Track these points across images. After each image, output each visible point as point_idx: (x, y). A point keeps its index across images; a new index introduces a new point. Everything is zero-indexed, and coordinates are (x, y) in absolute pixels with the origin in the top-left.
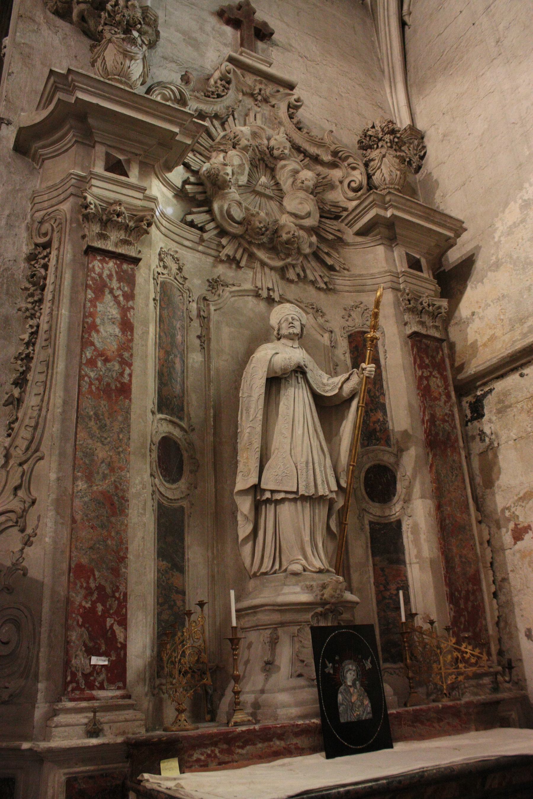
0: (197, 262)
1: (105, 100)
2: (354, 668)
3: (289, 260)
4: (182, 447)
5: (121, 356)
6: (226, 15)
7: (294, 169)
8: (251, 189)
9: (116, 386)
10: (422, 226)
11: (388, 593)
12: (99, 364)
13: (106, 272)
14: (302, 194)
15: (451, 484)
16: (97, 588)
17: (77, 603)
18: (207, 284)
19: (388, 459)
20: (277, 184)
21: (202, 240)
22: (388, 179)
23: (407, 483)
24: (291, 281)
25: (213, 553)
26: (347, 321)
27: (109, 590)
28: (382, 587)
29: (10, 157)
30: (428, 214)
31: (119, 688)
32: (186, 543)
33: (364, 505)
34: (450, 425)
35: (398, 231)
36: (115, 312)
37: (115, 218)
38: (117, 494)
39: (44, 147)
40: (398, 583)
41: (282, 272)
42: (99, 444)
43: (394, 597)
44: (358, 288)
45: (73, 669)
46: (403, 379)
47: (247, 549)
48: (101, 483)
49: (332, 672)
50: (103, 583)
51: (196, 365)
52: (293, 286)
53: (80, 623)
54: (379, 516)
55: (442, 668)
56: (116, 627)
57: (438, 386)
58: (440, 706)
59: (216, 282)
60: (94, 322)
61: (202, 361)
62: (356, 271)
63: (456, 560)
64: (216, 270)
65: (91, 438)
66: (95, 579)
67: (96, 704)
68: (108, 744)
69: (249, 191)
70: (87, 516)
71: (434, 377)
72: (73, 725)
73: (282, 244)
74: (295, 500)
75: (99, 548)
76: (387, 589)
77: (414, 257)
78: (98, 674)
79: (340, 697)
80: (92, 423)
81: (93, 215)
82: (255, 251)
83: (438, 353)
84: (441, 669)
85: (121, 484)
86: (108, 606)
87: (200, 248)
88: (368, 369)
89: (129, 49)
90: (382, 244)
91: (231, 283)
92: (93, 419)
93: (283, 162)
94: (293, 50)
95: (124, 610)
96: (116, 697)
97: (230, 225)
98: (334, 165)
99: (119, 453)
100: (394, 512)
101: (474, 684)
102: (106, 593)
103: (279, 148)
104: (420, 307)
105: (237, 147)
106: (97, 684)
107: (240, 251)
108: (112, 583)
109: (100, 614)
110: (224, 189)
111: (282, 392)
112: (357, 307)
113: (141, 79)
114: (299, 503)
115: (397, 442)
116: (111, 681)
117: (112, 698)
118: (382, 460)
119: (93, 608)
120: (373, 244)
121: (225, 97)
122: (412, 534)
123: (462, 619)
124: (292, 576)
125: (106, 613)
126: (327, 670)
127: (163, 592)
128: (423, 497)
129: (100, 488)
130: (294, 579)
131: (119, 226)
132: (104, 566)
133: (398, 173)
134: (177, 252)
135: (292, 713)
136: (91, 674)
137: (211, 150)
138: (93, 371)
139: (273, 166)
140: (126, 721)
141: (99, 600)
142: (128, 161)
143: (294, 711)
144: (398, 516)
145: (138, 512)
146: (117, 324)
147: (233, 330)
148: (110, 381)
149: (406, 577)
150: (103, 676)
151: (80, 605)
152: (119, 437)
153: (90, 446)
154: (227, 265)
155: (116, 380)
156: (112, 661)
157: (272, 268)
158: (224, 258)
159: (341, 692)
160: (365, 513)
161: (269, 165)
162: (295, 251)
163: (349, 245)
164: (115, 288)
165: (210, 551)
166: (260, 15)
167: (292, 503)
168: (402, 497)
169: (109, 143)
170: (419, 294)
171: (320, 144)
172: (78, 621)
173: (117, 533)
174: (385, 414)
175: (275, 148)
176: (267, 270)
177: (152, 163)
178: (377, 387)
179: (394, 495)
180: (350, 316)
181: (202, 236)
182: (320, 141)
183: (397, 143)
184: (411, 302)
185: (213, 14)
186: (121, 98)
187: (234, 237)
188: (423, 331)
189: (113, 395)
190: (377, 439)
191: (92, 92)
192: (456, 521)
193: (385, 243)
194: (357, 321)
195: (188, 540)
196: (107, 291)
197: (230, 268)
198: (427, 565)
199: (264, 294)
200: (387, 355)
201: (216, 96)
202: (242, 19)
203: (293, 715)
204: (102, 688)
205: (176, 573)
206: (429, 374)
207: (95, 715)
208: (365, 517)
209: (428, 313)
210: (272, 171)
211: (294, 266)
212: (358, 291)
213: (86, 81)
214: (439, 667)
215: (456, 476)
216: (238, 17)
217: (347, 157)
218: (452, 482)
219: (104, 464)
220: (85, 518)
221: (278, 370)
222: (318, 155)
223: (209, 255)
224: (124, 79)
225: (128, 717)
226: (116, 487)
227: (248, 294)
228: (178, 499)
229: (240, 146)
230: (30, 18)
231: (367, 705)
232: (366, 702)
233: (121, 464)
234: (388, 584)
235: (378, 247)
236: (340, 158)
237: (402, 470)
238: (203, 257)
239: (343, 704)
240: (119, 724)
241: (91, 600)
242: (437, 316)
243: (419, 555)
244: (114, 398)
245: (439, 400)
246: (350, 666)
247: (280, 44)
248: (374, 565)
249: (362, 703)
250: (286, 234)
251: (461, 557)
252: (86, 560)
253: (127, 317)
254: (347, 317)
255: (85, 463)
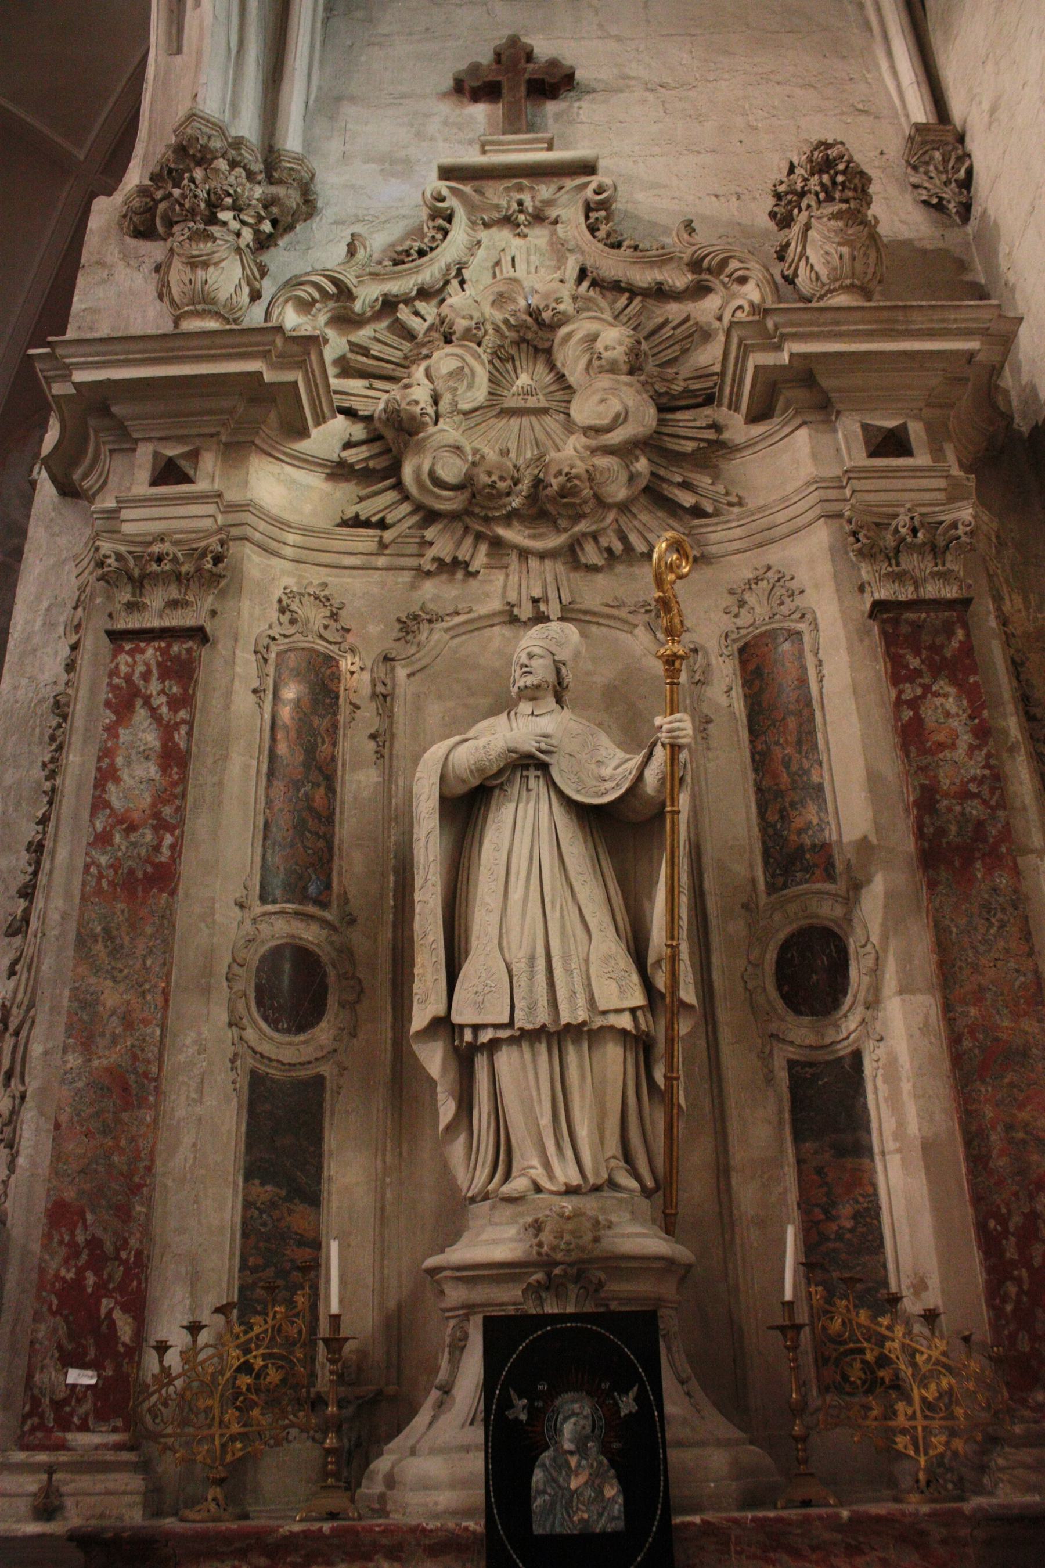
0: (375, 590)
1: (139, 365)
2: (587, 1411)
3: (582, 526)
4: (325, 959)
5: (157, 815)
6: (467, 87)
7: (587, 335)
8: (498, 409)
9: (145, 873)
10: (881, 353)
11: (835, 1228)
12: (117, 838)
13: (141, 668)
14: (605, 381)
15: (982, 949)
16: (88, 1243)
17: (52, 1272)
18: (399, 626)
19: (828, 911)
20: (561, 377)
21: (383, 546)
22: (823, 272)
23: (870, 962)
24: (594, 569)
25: (384, 1162)
26: (736, 616)
27: (109, 1247)
28: (818, 1214)
29: (54, 510)
30: (887, 321)
31: (115, 1430)
32: (326, 1147)
33: (774, 1027)
34: (985, 802)
35: (825, 383)
36: (151, 738)
37: (154, 567)
38: (135, 1071)
39: (85, 476)
40: (857, 1202)
41: (571, 555)
42: (109, 983)
43: (848, 1236)
44: (759, 538)
45: (36, 1392)
46: (854, 719)
47: (457, 1149)
48: (107, 1053)
49: (523, 1417)
50: (99, 1233)
51: (365, 794)
52: (600, 578)
53: (54, 1307)
54: (811, 1047)
55: (919, 1414)
56: (117, 1315)
57: (947, 714)
58: (845, 1513)
59: (416, 618)
60: (112, 764)
61: (378, 783)
62: (752, 503)
63: (994, 1137)
64: (416, 595)
65: (96, 974)
66: (85, 1227)
67: (63, 1457)
68: (52, 1535)
69: (494, 413)
70: (78, 1115)
71: (937, 695)
72: (10, 1495)
73: (553, 500)
74: (512, 1041)
75: (96, 1170)
76: (830, 1218)
77: (880, 429)
78: (78, 1401)
79: (538, 1476)
80: (100, 946)
81: (115, 576)
82: (501, 531)
83: (950, 634)
84: (913, 1417)
85: (143, 1050)
86: (105, 1277)
87: (381, 561)
88: (665, 727)
89: (195, 253)
90: (804, 423)
91: (450, 610)
92: (100, 939)
93: (564, 331)
94: (633, 83)
95: (135, 1283)
96: (105, 1446)
97: (439, 497)
98: (700, 290)
99: (143, 994)
100: (844, 1034)
101: (1029, 1460)
102: (103, 1251)
103: (547, 306)
104: (890, 541)
105: (454, 338)
106: (75, 1420)
107: (469, 541)
108: (115, 1233)
109: (90, 1290)
110: (417, 433)
111: (491, 816)
112: (757, 580)
113: (246, 290)
114: (525, 1046)
115: (848, 866)
116: (102, 1415)
117: (97, 1447)
118: (817, 917)
119: (79, 1281)
120: (787, 430)
121: (439, 250)
122: (885, 1082)
123: (1012, 1289)
124: (504, 1204)
125: (102, 1289)
126: (510, 1414)
127: (261, 1245)
128: (903, 990)
129: (105, 1062)
130: (509, 1210)
131: (164, 579)
132: (104, 1203)
133: (845, 250)
134: (325, 585)
135: (436, 1504)
136: (66, 1401)
137: (406, 363)
138: (104, 853)
139: (546, 345)
140: (108, 1493)
141: (91, 1265)
142: (194, 456)
143: (445, 1499)
144: (854, 1042)
145: (188, 1097)
146: (153, 756)
147: (450, 704)
148: (134, 865)
149: (874, 1186)
150: (87, 1406)
151: (57, 1276)
152: (144, 963)
153: (92, 989)
154: (444, 577)
155: (146, 861)
156: (107, 1379)
157: (542, 556)
158: (433, 567)
159: (544, 1465)
160: (774, 1043)
161: (540, 347)
162: (592, 503)
163: (739, 450)
164: (154, 693)
165: (379, 1158)
166: (544, 48)
167: (515, 1048)
168: (861, 996)
169: (158, 435)
170: (890, 510)
171: (663, 259)
172: (51, 1305)
173: (132, 1139)
174: (822, 807)
175: (541, 307)
176: (534, 563)
177: (250, 439)
178: (805, 748)
179: (845, 994)
180: (742, 603)
181: (381, 537)
182: (661, 252)
183: (843, 183)
184: (861, 536)
185: (445, 95)
186: (145, 351)
187: (454, 516)
188: (906, 594)
189: (140, 889)
190: (807, 869)
191: (97, 363)
192: (997, 1039)
193: (809, 419)
194: (758, 610)
195: (331, 1140)
196: (139, 702)
197: (451, 581)
198: (917, 1154)
199: (525, 612)
200: (825, 672)
201: (415, 256)
202: (499, 78)
203: (440, 1508)
204: (84, 1427)
205: (300, 1208)
206: (919, 691)
207: (50, 1479)
208: (775, 1052)
209: (920, 549)
210: (545, 353)
211: (595, 536)
212: (761, 545)
213: (81, 349)
214: (910, 1412)
215: (1002, 926)
216: (490, 78)
217: (724, 262)
218: (985, 941)
219: (114, 1018)
220: (76, 1119)
221: (466, 775)
222: (660, 284)
223: (403, 569)
224: (199, 307)
225: (111, 1486)
226: (135, 1057)
227: (490, 622)
228: (309, 1063)
229: (457, 335)
230: (98, 263)
231: (613, 1500)
232: (611, 1491)
233: (145, 1015)
234: (834, 1204)
235: (797, 432)
236: (709, 270)
237: (859, 931)
238: (389, 577)
239: (544, 1492)
240: (94, 1499)
241: (76, 1266)
242: (947, 547)
243: (900, 1134)
244: (140, 894)
245: (953, 746)
246: (576, 1407)
247: (599, 86)
248: (799, 1161)
249: (600, 1492)
250: (556, 477)
251: (1009, 1128)
252: (73, 1194)
253: (174, 742)
254: (735, 610)
255: (80, 1020)
